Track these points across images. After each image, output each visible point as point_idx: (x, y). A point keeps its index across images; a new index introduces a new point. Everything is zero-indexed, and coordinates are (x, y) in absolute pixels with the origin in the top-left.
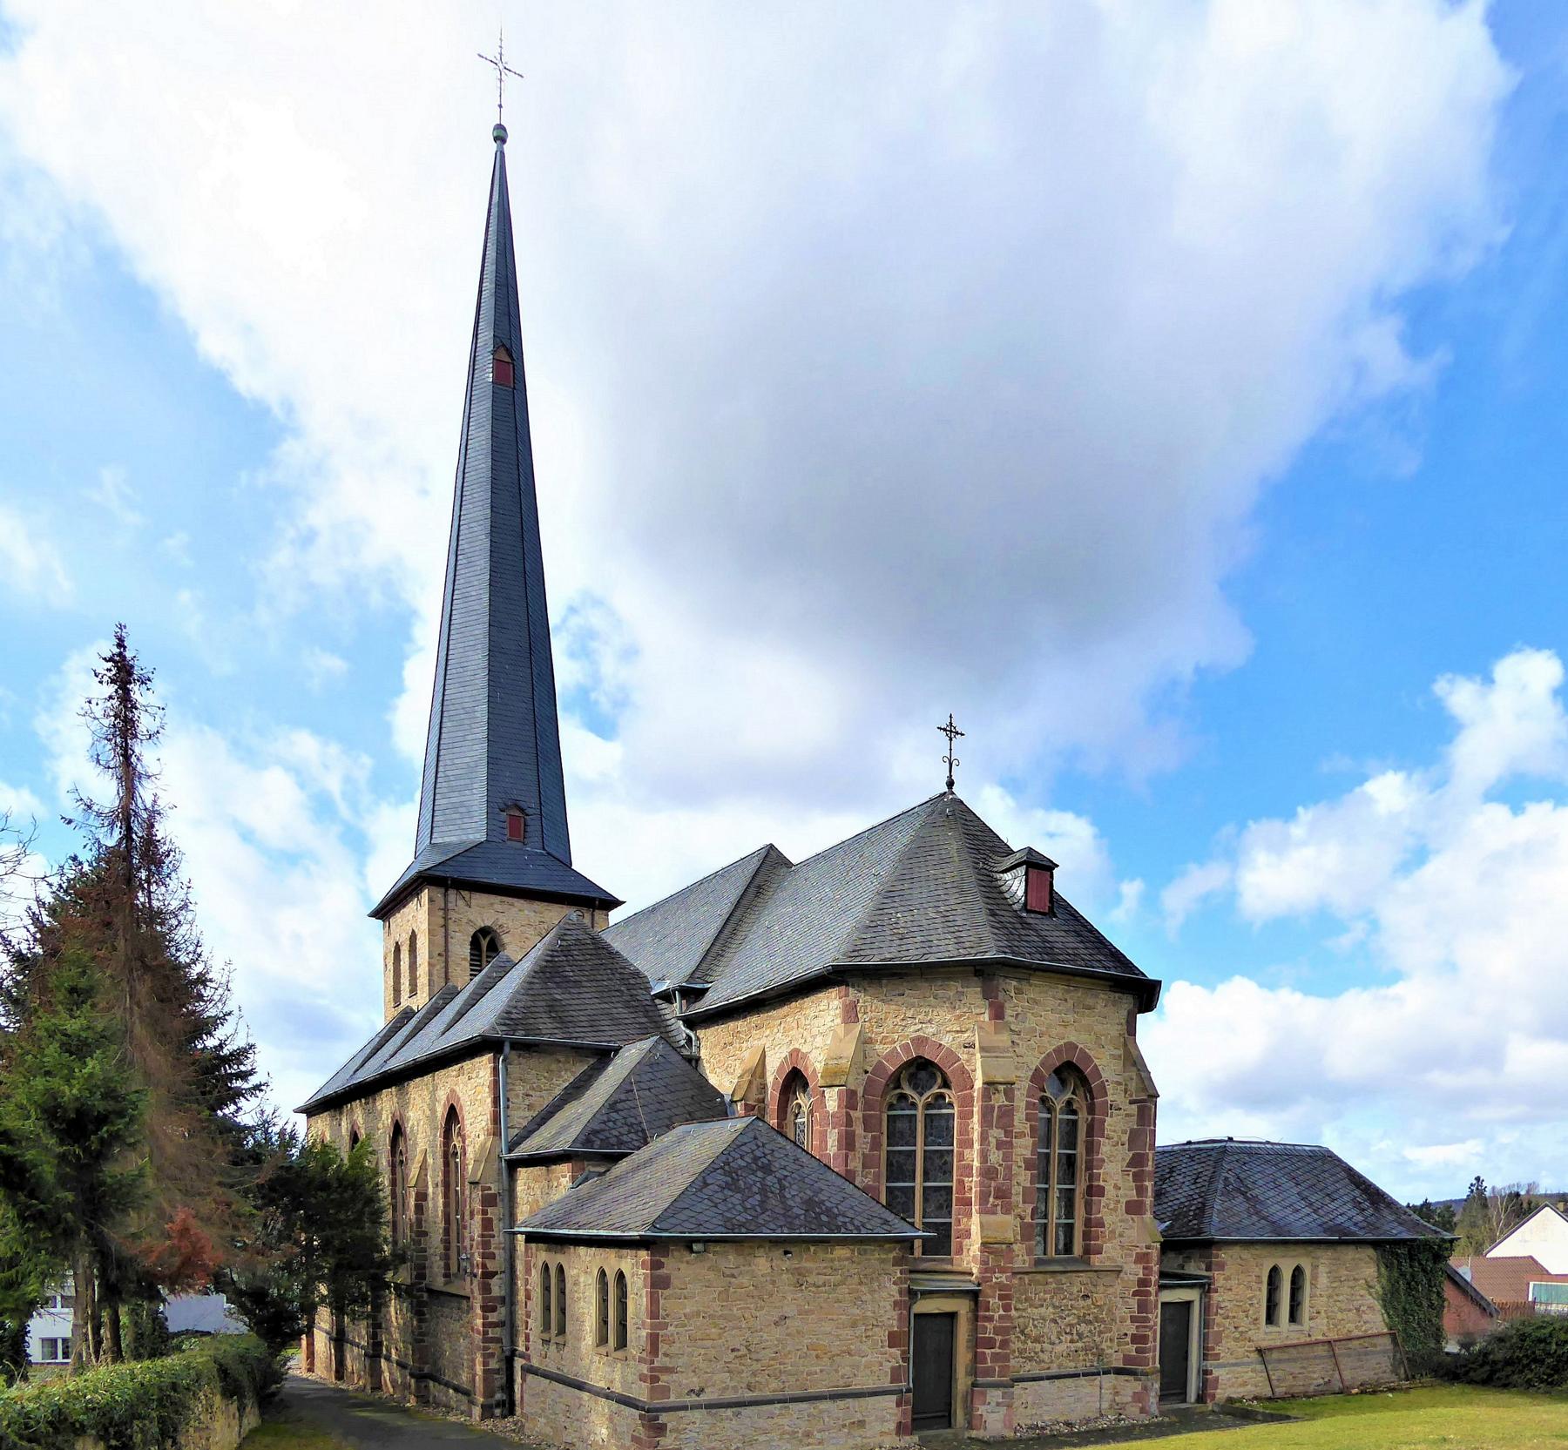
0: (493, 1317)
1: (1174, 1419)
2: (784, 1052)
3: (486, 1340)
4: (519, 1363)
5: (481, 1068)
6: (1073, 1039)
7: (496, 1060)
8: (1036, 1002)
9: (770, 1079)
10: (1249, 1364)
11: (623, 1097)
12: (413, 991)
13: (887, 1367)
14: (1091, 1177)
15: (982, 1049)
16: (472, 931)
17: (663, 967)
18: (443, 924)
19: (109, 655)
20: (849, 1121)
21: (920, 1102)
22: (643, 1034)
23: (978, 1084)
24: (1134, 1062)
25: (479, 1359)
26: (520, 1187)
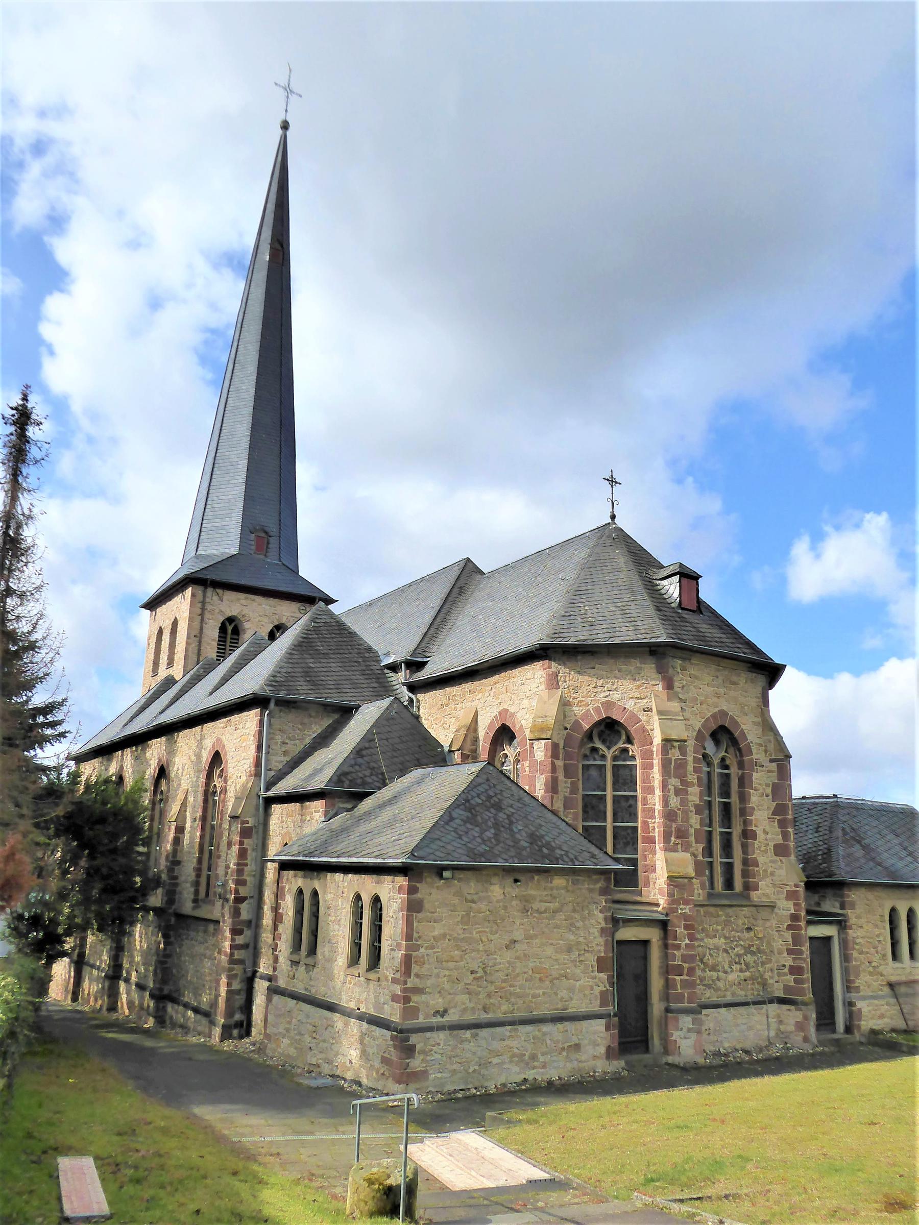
0: (240, 940)
1: (832, 1049)
2: (495, 712)
3: (232, 961)
4: (261, 986)
5: (250, 719)
6: (725, 708)
7: (262, 715)
8: (696, 677)
9: (481, 733)
10: (882, 997)
11: (367, 745)
12: (170, 663)
13: (597, 990)
14: (746, 823)
15: (660, 713)
16: (222, 619)
17: (391, 643)
18: (200, 613)
19: (14, 405)
20: (554, 769)
21: (609, 754)
22: (379, 696)
23: (657, 740)
24: (769, 727)
25: (224, 980)
26: (274, 822)
